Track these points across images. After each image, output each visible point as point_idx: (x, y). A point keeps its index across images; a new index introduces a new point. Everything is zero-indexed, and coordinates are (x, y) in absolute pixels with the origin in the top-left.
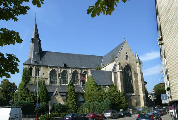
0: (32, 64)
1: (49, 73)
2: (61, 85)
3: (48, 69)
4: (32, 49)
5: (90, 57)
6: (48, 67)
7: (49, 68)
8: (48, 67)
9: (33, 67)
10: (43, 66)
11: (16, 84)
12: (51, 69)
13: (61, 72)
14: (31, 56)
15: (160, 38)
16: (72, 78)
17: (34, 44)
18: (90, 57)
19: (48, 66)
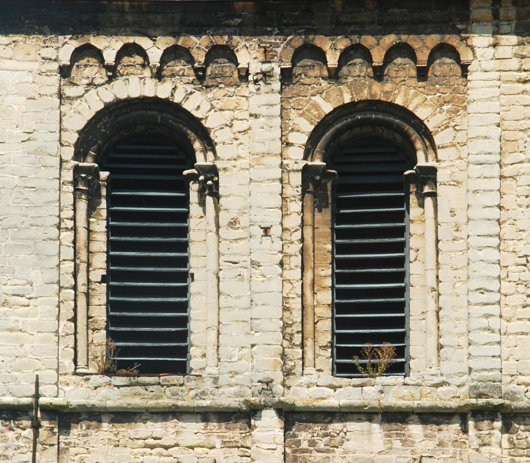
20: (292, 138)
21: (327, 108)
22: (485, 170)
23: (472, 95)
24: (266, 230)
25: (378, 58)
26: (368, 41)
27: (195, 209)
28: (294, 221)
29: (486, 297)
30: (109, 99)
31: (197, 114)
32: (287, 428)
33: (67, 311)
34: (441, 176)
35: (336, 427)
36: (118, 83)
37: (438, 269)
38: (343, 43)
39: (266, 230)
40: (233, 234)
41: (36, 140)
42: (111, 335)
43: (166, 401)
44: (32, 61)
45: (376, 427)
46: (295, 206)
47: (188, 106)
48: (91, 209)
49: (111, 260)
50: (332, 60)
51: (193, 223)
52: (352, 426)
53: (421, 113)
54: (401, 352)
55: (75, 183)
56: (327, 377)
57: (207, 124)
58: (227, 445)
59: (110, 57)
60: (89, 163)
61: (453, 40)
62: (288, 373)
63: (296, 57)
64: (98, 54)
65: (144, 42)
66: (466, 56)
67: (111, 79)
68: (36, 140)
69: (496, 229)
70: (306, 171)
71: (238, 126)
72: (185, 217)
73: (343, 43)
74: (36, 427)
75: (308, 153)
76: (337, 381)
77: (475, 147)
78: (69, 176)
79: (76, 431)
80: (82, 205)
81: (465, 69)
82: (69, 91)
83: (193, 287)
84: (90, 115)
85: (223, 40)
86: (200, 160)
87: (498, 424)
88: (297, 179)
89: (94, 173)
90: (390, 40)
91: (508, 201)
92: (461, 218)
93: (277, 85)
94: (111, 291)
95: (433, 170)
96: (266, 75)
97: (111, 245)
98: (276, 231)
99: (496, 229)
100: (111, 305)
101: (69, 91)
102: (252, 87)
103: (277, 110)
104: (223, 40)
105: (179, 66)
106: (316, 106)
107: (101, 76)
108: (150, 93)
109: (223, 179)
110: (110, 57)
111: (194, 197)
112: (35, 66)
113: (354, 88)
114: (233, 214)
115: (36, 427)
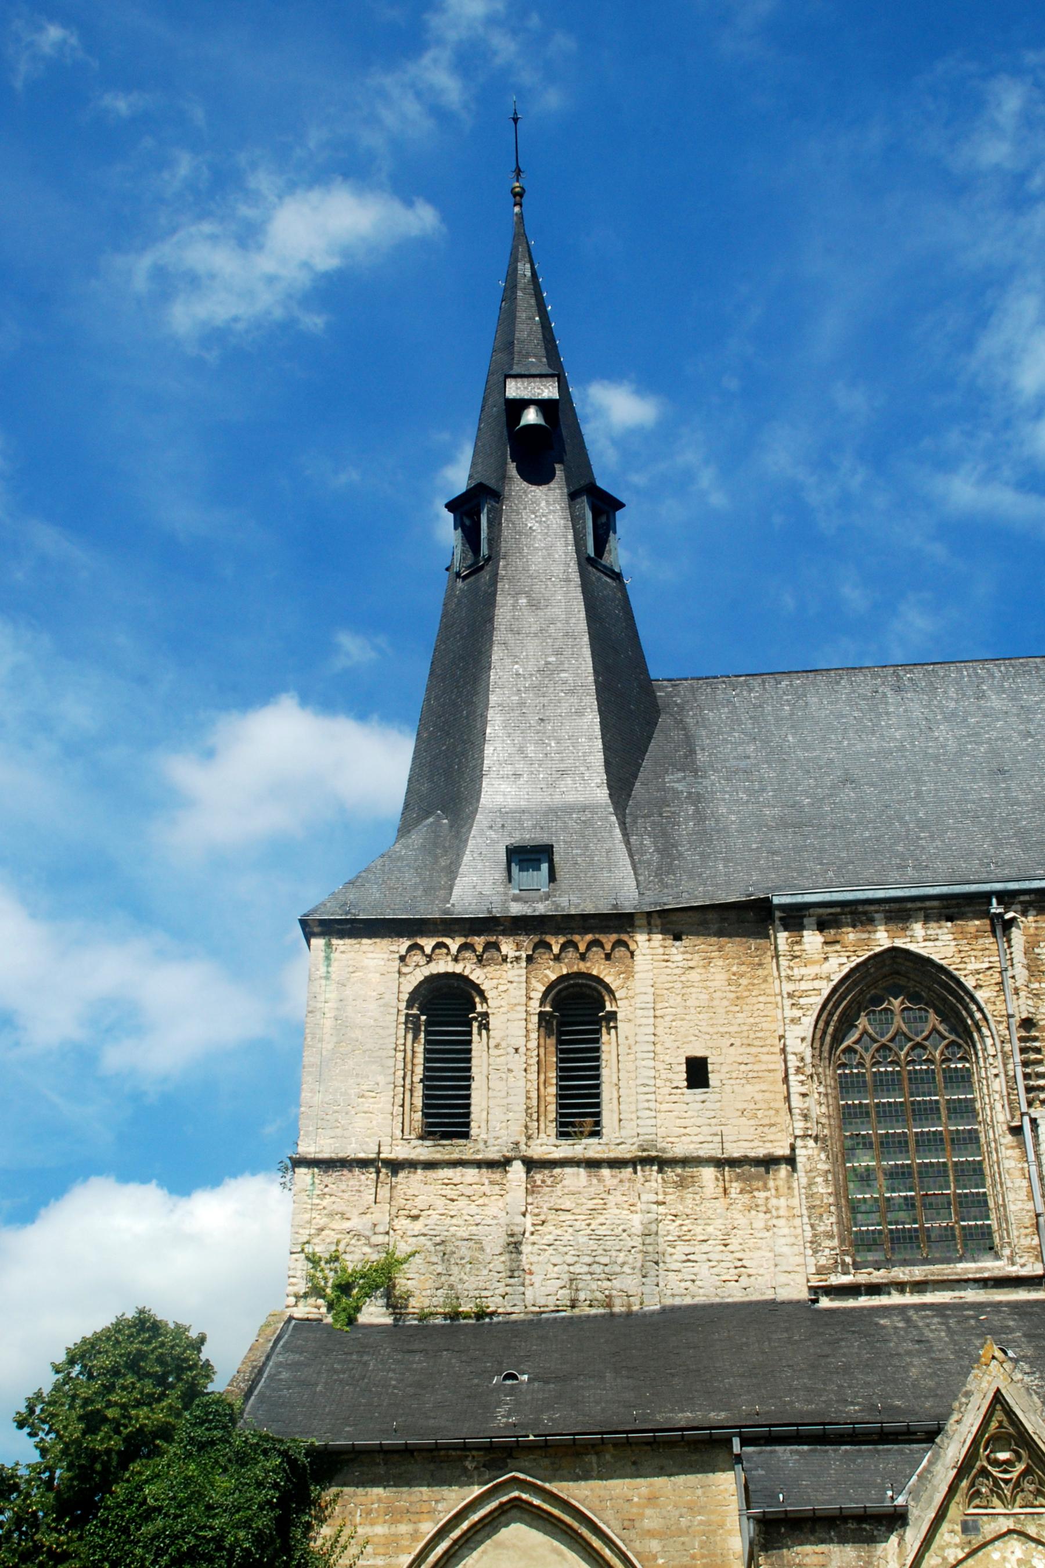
21: (553, 977)
25: (582, 948)
26: (576, 938)
28: (533, 1044)
32: (528, 1172)
33: (398, 1100)
35: (557, 1171)
36: (433, 964)
38: (562, 940)
43: (455, 1156)
45: (582, 1171)
48: (415, 1038)
50: (556, 949)
52: (568, 1170)
53: (608, 980)
54: (598, 1123)
55: (406, 1023)
56: (553, 1140)
58: (492, 1183)
60: (415, 1011)
61: (625, 937)
62: (529, 1138)
63: (536, 947)
64: (421, 948)
65: (448, 941)
66: (633, 947)
70: (541, 1014)
73: (562, 940)
74: (378, 1172)
75: (542, 1003)
77: (639, 999)
78: (402, 1019)
79: (402, 1175)
80: (410, 1036)
82: (405, 970)
83: (474, 1085)
85: (493, 939)
89: (417, 1017)
90: (589, 937)
91: (660, 1031)
92: (631, 1041)
96: (518, 959)
101: (405, 970)
104: (493, 939)
105: (468, 954)
107: (423, 961)
109: (491, 1019)
110: (428, 950)
113: (568, 965)
115: (378, 1172)
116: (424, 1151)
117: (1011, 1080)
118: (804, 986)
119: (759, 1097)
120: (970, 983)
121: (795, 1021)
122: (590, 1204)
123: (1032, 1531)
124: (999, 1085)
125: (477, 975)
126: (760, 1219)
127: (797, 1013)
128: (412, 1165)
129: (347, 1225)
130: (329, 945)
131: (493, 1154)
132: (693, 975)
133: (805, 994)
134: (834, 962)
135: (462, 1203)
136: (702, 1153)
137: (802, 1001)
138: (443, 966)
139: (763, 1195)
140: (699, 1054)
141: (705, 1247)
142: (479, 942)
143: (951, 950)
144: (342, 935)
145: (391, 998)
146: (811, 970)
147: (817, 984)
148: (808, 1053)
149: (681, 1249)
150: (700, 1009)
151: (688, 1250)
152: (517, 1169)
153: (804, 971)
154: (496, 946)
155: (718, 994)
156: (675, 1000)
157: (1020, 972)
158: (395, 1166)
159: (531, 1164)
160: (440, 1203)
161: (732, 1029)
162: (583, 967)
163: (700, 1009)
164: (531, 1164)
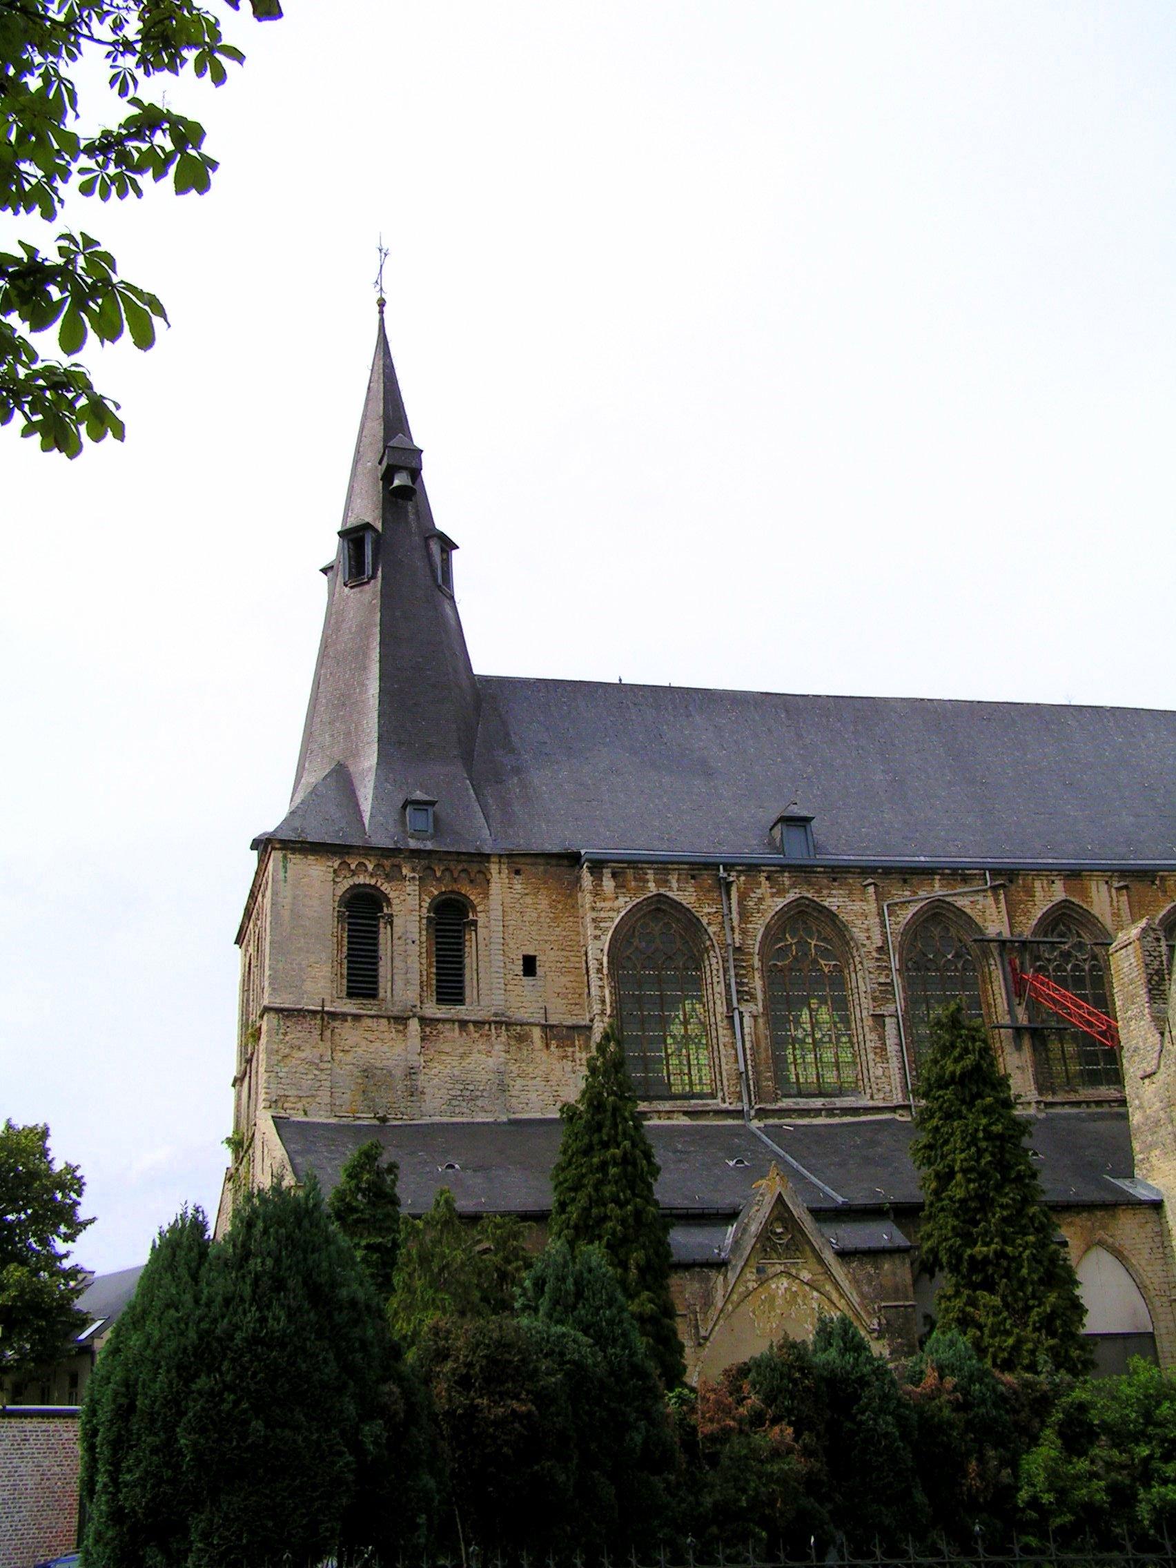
0: (381, 840)
1: (598, 949)
2: (1031, 983)
3: (586, 899)
4: (364, 652)
5: (349, 1018)
6: (587, 879)
7: (597, 892)
8: (587, 879)
9: (394, 875)
10: (517, 861)
11: (50, 1153)
12: (624, 904)
13: (758, 927)
14: (351, 736)
15: (372, 1276)
16: (899, 1004)
17: (385, 595)
18: (349, 1018)
19: (574, 859)
20: (423, 904)
22: (497, 923)
23: (491, 892)
24: (413, 942)
27: (382, 930)
28: (424, 939)
29: (498, 975)
30: (352, 883)
31: (386, 892)
34: (479, 924)
37: (286, 872)
39: (413, 942)
40: (400, 942)
41: (20, 242)
42: (349, 981)
44: (221, 1202)
46: (424, 933)
47: (382, 888)
49: (349, 949)
51: (381, 937)
53: (472, 897)
57: (390, 896)
59: (353, 867)
60: (342, 909)
65: (367, 863)
67: (353, 875)
68: (20, 242)
69: (502, 947)
71: (402, 898)
72: (377, 932)
75: (429, 911)
76: (440, 1007)
78: (336, 914)
81: (488, 881)
82: (338, 880)
84: (344, 890)
86: (385, 909)
87: (504, 1028)
88: (424, 921)
93: (417, 883)
94: (349, 962)
95: (476, 921)
97: (349, 943)
98: (418, 942)
99: (502, 947)
100: (349, 968)
101: (338, 880)
102: (407, 883)
103: (417, 893)
106: (432, 892)
108: (367, 882)
109: (395, 919)
110: (353, 867)
111: (382, 925)
112: (324, 869)
113: (446, 886)
114: (400, 934)
116: (350, 1007)
117: (728, 986)
118: (603, 914)
119: (569, 985)
120: (705, 921)
121: (597, 938)
122: (461, 1050)
123: (794, 1272)
124: (720, 988)
125: (385, 887)
126: (569, 1065)
127: (598, 932)
128: (343, 1017)
129: (303, 1055)
130: (285, 857)
131: (396, 1011)
132: (529, 900)
133: (603, 920)
134: (622, 900)
135: (378, 1044)
136: (531, 1020)
137: (602, 925)
138: (361, 879)
139: (571, 1049)
140: (532, 953)
141: (534, 1082)
142: (387, 863)
143: (693, 899)
144: (294, 851)
145: (329, 897)
146: (608, 904)
147: (611, 914)
148: (605, 959)
149: (519, 1082)
150: (532, 923)
151: (525, 1083)
152: (414, 1025)
153: (603, 904)
154: (399, 867)
155: (543, 914)
156: (517, 916)
157: (735, 915)
158: (333, 1015)
159: (423, 1021)
160: (364, 1043)
161: (552, 938)
162: (455, 887)
163: (532, 923)
164: (423, 1021)
